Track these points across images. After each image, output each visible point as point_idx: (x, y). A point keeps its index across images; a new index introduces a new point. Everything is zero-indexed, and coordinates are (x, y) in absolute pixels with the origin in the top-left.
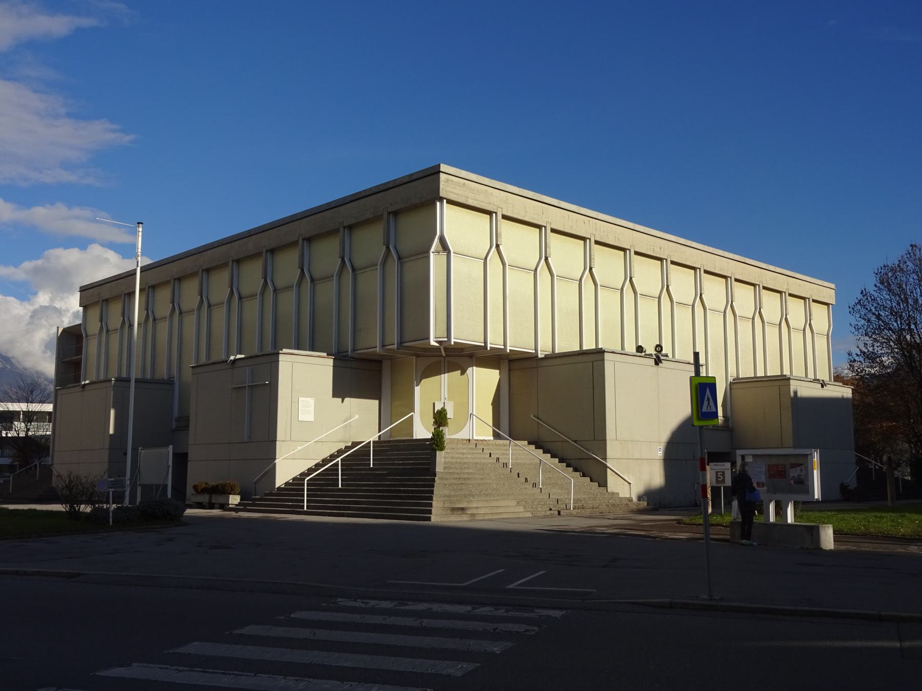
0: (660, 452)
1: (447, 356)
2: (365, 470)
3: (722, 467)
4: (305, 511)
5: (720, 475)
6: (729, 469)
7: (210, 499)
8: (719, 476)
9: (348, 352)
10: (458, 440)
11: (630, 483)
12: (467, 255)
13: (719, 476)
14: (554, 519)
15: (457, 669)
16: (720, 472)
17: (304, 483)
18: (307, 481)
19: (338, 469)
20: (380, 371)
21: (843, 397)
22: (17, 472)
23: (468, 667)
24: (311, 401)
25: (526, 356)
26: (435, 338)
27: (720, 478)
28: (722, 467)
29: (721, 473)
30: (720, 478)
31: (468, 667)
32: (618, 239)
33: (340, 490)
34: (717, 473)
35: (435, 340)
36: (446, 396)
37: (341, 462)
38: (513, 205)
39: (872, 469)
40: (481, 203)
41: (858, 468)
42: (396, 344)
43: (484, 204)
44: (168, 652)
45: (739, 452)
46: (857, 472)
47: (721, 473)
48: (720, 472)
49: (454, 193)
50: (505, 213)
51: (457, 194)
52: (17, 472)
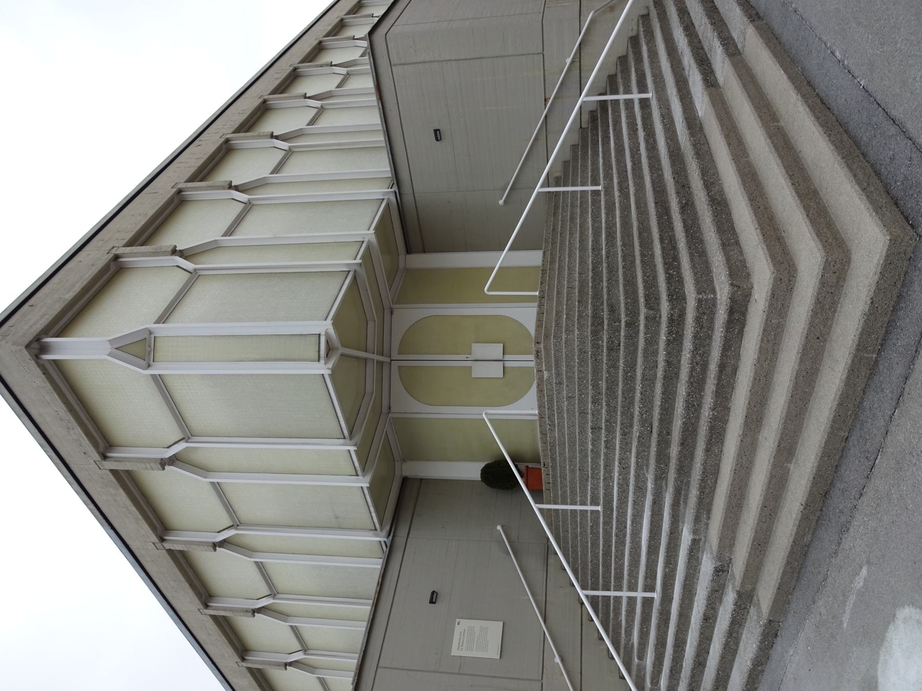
4: (604, 507)
9: (380, 541)
20: (422, 479)
24: (462, 626)
26: (319, 361)
35: (322, 361)
36: (463, 357)
37: (587, 589)
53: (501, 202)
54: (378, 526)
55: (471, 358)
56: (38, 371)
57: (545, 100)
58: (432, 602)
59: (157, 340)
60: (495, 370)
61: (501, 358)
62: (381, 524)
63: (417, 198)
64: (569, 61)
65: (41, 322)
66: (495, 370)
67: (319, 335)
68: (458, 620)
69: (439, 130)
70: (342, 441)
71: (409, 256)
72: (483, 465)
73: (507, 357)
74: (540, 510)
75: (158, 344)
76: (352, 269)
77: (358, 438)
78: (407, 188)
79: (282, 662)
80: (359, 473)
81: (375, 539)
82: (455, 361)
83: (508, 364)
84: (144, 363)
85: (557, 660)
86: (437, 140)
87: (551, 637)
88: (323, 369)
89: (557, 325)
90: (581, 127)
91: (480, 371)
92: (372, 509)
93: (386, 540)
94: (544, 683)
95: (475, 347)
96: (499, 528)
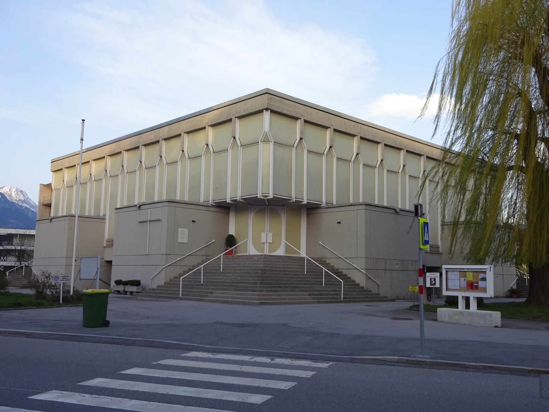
0: (397, 266)
1: (269, 205)
2: (218, 273)
3: (434, 276)
4: (181, 297)
5: (433, 280)
6: (438, 277)
7: (124, 288)
8: (432, 281)
9: (209, 201)
10: (274, 256)
11: (378, 285)
12: (340, 158)
13: (432, 281)
14: (243, 328)
15: (257, 399)
16: (433, 278)
17: (180, 281)
18: (182, 279)
19: (201, 273)
20: (229, 213)
21: (135, 280)
22: (16, 268)
23: (267, 397)
24: (186, 231)
25: (313, 206)
26: (262, 194)
27: (433, 282)
28: (434, 276)
29: (434, 279)
30: (433, 282)
31: (267, 397)
32: (375, 136)
33: (202, 285)
34: (431, 279)
35: (262, 195)
36: (268, 230)
37: (203, 268)
38: (311, 115)
39: (526, 278)
40: (292, 113)
41: (517, 278)
42: (238, 197)
43: (293, 113)
44: (120, 373)
45: (444, 267)
46: (516, 280)
47: (434, 279)
48: (433, 278)
49: (275, 106)
50: (386, 143)
51: (277, 107)
52: (16, 268)
53: (320, 242)
54: (214, 202)
55: (268, 232)
56: (261, 108)
57: (346, 258)
58: (193, 221)
59: (269, 144)
60: (264, 240)
61: (267, 242)
62: (214, 203)
63: (322, 214)
64: (355, 266)
65: (275, 108)
66: (264, 240)
67: (269, 194)
68: (188, 229)
69: (340, 223)
70: (240, 196)
71: (306, 209)
72: (234, 235)
73: (268, 244)
74: (221, 256)
75: (268, 144)
76: (292, 198)
77: (241, 200)
78: (325, 210)
79: (162, 154)
80: (231, 199)
81: (211, 200)
82: (267, 227)
83: (265, 244)
84: (262, 141)
85: (178, 259)
86: (337, 223)
87: (184, 257)
88: (260, 196)
89: (267, 261)
90: (338, 269)
91: (263, 235)
92: (220, 201)
93: (210, 204)
94: (412, 321)
95: (271, 233)
96: (214, 241)
